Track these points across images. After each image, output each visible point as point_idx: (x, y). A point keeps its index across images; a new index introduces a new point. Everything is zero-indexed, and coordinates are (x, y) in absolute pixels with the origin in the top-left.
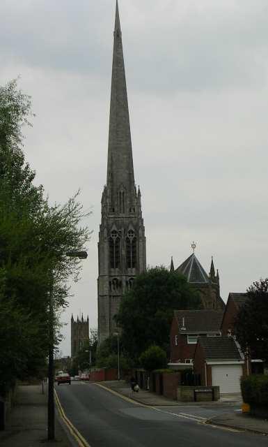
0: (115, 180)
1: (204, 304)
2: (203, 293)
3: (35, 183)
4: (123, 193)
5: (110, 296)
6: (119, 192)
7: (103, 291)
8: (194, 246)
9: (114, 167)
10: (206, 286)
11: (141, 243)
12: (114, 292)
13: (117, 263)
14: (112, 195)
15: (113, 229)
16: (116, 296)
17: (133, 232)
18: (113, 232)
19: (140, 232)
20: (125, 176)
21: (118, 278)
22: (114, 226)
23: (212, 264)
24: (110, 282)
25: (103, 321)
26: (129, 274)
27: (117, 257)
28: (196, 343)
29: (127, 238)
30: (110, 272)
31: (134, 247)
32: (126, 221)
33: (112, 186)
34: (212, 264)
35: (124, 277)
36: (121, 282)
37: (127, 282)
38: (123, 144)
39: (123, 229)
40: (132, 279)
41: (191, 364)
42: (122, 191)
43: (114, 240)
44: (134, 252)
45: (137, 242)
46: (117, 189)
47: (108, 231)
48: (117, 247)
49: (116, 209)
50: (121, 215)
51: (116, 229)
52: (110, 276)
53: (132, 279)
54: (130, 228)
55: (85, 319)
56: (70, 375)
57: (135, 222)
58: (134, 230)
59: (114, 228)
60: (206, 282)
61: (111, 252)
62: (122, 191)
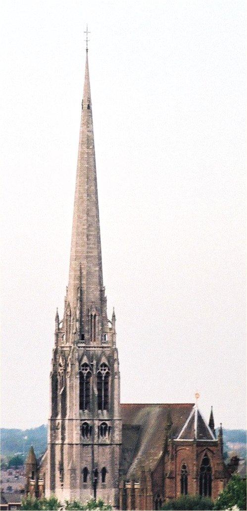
0: (85, 297)
1: (212, 465)
2: (212, 452)
3: (58, 501)
4: (95, 316)
6: (90, 314)
8: (221, 424)
10: (215, 444)
11: (116, 381)
13: (88, 403)
14: (81, 317)
15: (83, 363)
16: (86, 445)
17: (105, 365)
18: (83, 366)
19: (116, 366)
20: (97, 293)
21: (88, 422)
25: (54, 435)
26: (101, 418)
27: (88, 396)
28: (192, 440)
29: (100, 373)
31: (106, 383)
32: (99, 351)
33: (81, 305)
39: (95, 362)
40: (104, 424)
41: (178, 440)
42: (93, 314)
43: (85, 375)
44: (106, 390)
46: (88, 311)
49: (86, 336)
50: (92, 344)
52: (81, 420)
53: (104, 424)
54: (104, 360)
57: (108, 352)
58: (107, 363)
59: (85, 360)
60: (214, 440)
62: (93, 314)
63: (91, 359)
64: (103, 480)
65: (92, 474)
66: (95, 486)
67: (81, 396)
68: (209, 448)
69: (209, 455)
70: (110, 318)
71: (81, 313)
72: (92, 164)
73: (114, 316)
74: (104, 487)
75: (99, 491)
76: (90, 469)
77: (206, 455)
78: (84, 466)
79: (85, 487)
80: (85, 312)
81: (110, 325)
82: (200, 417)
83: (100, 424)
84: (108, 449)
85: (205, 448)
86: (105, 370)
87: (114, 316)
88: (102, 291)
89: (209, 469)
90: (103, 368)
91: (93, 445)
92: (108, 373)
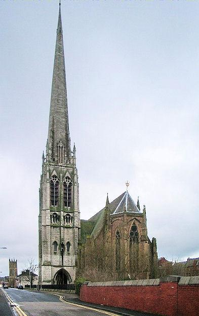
0: (55, 136)
5: (51, 227)
7: (45, 222)
8: (127, 185)
9: (55, 127)
11: (75, 187)
12: (56, 223)
15: (53, 174)
17: (56, 177)
18: (53, 177)
21: (57, 213)
22: (67, 173)
23: (108, 199)
24: (51, 215)
27: (57, 197)
30: (51, 208)
31: (70, 190)
34: (108, 199)
35: (62, 212)
36: (60, 216)
37: (64, 217)
38: (63, 110)
45: (72, 187)
47: (50, 175)
48: (57, 189)
49: (56, 159)
51: (56, 174)
54: (67, 175)
55: (15, 261)
56: (87, 227)
58: (70, 177)
59: (54, 173)
61: (52, 193)
63: (59, 173)
64: (68, 250)
65: (60, 246)
66: (62, 254)
67: (52, 196)
68: (137, 218)
69: (137, 223)
70: (72, 150)
71: (53, 145)
72: (62, 61)
73: (74, 148)
74: (69, 254)
75: (66, 258)
76: (59, 243)
77: (134, 223)
78: (53, 240)
79: (55, 253)
80: (55, 144)
81: (72, 155)
82: (130, 199)
83: (65, 215)
84: (71, 231)
85: (133, 218)
86: (56, 180)
87: (74, 148)
88: (67, 135)
89: (137, 234)
90: (68, 180)
91: (60, 227)
92: (57, 182)
